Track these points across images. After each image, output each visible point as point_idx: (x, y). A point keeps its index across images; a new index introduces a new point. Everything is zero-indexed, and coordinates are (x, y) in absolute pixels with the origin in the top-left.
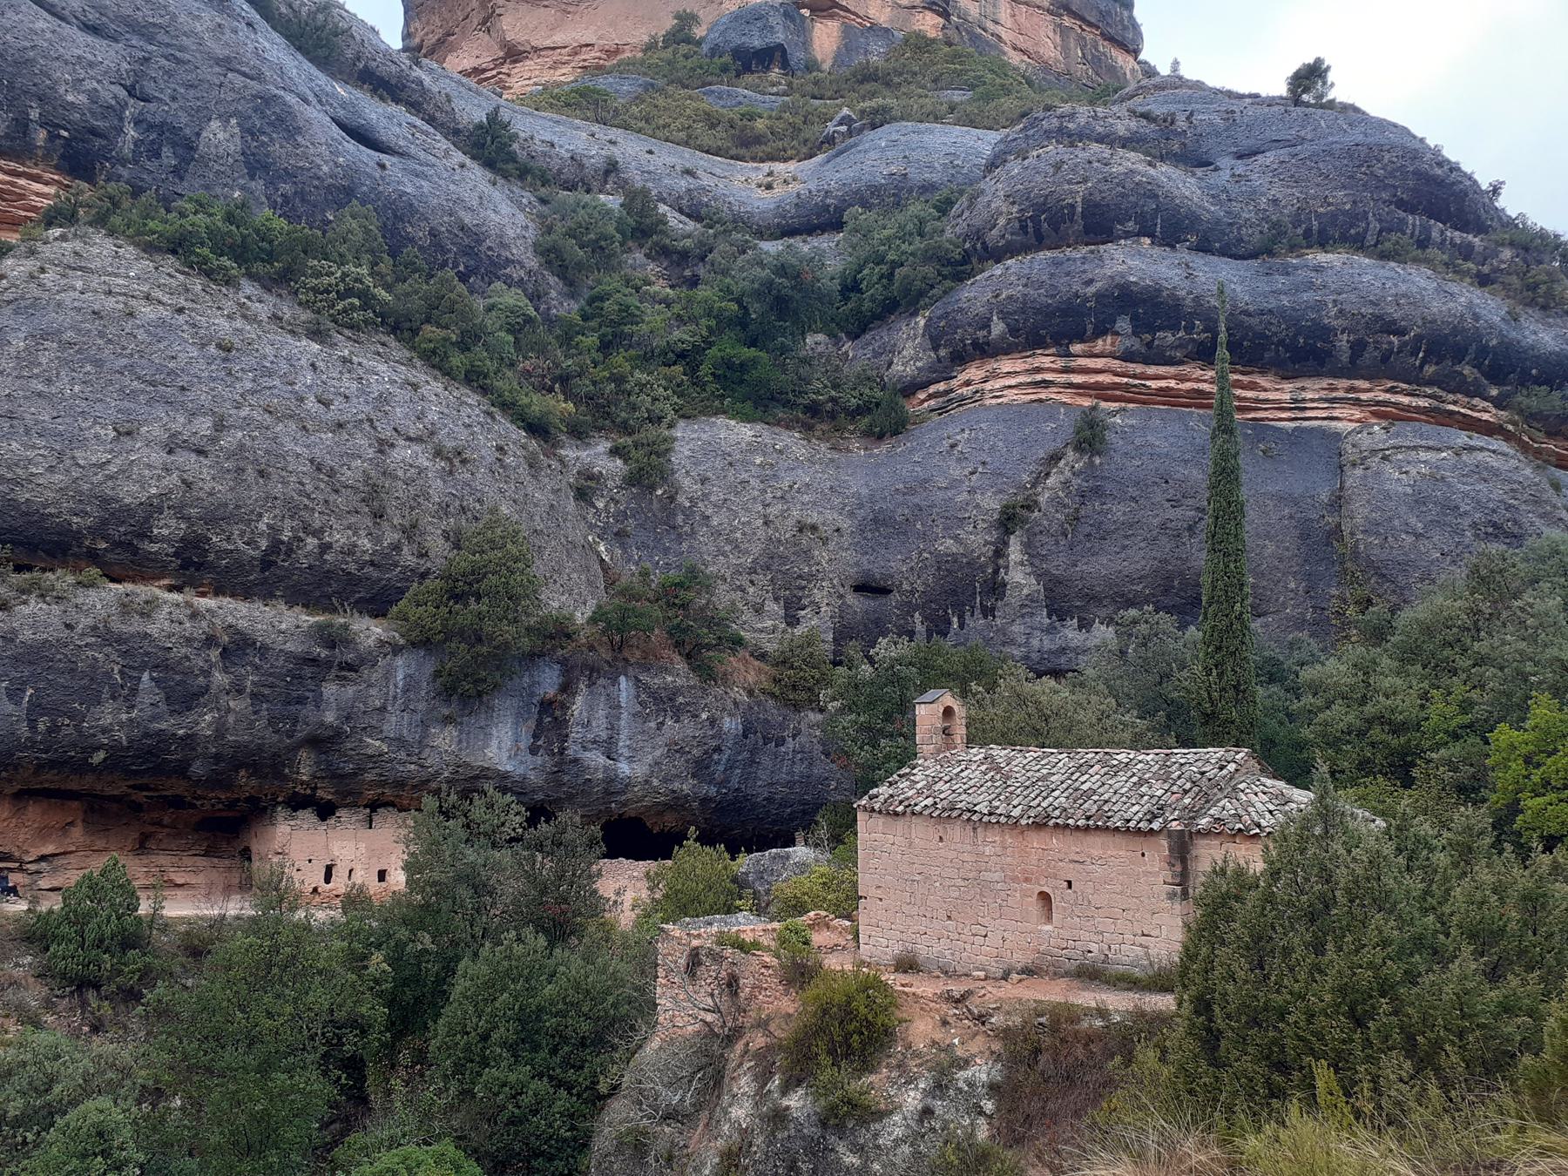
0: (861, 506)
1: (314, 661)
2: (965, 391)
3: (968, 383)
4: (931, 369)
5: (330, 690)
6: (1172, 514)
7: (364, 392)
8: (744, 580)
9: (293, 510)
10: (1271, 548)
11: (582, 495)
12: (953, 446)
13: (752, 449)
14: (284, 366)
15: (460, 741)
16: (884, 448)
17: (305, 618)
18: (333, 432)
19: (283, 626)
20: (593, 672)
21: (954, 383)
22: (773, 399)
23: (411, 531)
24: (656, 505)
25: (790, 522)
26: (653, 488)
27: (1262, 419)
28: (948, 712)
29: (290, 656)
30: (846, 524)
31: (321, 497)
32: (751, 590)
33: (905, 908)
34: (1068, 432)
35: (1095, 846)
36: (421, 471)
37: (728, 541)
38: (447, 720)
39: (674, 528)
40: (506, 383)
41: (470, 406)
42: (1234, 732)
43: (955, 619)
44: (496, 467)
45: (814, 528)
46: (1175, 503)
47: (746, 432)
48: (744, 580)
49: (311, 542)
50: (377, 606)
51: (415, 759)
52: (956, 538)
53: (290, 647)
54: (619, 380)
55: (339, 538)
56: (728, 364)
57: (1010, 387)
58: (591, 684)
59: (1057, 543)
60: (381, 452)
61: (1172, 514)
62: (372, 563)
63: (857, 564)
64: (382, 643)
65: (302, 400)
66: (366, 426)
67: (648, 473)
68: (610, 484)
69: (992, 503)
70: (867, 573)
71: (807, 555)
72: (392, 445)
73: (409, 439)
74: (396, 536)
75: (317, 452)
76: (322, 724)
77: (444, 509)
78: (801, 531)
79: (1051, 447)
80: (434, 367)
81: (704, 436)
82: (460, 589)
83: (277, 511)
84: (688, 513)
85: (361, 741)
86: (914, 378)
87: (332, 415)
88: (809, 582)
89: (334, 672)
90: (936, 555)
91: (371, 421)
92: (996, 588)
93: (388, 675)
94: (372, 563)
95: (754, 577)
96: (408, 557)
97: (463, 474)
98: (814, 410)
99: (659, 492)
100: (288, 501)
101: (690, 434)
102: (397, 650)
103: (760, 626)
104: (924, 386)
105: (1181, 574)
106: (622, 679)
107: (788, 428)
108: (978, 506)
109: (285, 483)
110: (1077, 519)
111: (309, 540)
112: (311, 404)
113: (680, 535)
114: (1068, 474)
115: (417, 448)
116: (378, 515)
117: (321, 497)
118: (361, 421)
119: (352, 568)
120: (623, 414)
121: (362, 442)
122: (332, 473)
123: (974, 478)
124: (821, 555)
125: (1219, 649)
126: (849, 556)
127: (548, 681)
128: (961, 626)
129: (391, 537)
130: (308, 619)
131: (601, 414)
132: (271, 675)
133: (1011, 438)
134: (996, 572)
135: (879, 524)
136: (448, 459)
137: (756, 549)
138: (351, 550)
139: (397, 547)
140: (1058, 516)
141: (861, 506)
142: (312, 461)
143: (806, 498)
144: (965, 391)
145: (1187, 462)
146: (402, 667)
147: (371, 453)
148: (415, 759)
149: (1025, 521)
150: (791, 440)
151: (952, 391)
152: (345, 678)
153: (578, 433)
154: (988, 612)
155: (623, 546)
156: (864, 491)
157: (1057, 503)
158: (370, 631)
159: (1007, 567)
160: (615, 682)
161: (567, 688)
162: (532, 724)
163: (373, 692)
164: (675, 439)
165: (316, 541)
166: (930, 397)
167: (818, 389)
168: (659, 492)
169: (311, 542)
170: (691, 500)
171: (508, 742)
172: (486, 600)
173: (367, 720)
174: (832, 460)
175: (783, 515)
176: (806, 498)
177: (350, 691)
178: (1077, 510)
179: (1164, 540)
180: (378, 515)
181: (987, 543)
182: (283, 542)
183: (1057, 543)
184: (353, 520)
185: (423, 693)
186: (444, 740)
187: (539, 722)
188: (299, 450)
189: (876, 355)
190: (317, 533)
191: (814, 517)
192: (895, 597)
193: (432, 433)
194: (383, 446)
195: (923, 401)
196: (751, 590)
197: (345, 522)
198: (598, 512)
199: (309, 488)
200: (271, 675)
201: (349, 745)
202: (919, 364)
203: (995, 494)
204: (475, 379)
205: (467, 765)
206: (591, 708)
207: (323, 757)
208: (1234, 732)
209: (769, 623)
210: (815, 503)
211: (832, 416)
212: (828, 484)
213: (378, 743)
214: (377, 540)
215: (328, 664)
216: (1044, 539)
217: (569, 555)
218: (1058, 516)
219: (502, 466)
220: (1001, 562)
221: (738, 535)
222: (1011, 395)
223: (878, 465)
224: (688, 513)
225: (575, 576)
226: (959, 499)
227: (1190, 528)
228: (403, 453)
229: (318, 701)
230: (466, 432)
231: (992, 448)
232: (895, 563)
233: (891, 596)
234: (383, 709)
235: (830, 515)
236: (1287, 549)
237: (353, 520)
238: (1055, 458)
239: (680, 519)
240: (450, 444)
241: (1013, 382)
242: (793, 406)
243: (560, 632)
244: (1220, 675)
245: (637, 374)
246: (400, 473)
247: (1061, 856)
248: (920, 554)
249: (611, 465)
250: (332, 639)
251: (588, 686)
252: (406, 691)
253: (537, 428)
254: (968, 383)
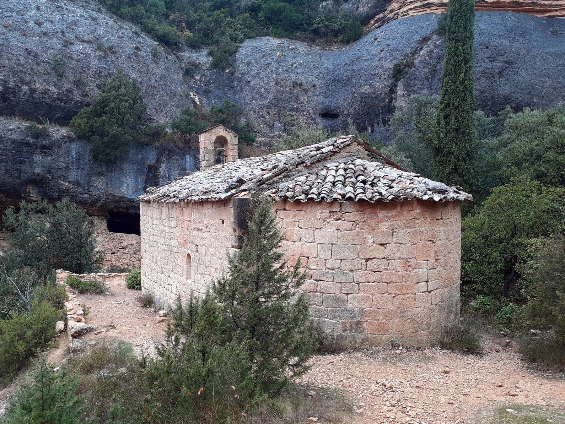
0: (328, 74)
1: (27, 144)
2: (391, 15)
3: (392, 11)
4: (375, 7)
5: (38, 158)
6: (488, 65)
7: (63, 20)
8: (264, 112)
9: (15, 73)
10: (549, 82)
11: (188, 73)
12: (375, 39)
13: (276, 48)
14: (21, 7)
15: (107, 184)
16: (348, 47)
17: (23, 124)
18: (40, 37)
19: (11, 127)
20: (170, 153)
21: (387, 12)
22: (298, 28)
23: (78, 84)
24: (225, 77)
25: (289, 82)
26: (224, 69)
27: (554, 16)
28: (221, 141)
29: (14, 141)
30: (319, 82)
31: (29, 66)
32: (268, 117)
34: (435, 26)
36: (87, 56)
37: (258, 93)
38: (101, 174)
39: (233, 88)
40: (151, 22)
41: (126, 29)
42: (453, 159)
43: (369, 128)
44: (133, 56)
45: (301, 85)
46: (491, 59)
47: (276, 42)
48: (264, 112)
49: (25, 88)
50: (64, 121)
51: (86, 191)
52: (370, 85)
53: (14, 137)
54: (218, 22)
55: (39, 86)
56: (274, 12)
57: (411, 9)
58: (169, 158)
59: (423, 84)
60: (65, 46)
61: (488, 65)
62: (59, 99)
63: (323, 103)
64: (64, 137)
65: (26, 22)
66: (60, 35)
67: (223, 62)
68: (204, 68)
69: (389, 64)
70: (328, 107)
71: (297, 98)
72: (72, 44)
73: (84, 41)
74: (70, 86)
75: (29, 46)
76: (34, 174)
77: (98, 74)
78: (294, 87)
79: (424, 33)
80: (114, 13)
81: (255, 45)
82: (101, 109)
83: (5, 73)
84: (240, 81)
85: (58, 182)
86: (368, 13)
87: (43, 28)
88: (297, 112)
89: (39, 150)
90: (360, 94)
91: (63, 32)
92: (390, 110)
93: (68, 152)
94: (59, 99)
95: (269, 110)
96: (77, 95)
97: (112, 58)
98: (317, 33)
99: (227, 71)
100: (11, 68)
101: (249, 44)
102: (71, 140)
103: (272, 134)
104: (373, 16)
105: (493, 98)
106: (188, 156)
107: (301, 41)
108: (382, 67)
109: (10, 59)
110: (435, 71)
111: (24, 87)
112: (31, 24)
113: (235, 91)
114: (432, 47)
115: (87, 46)
116: (61, 76)
117: (29, 66)
118: (57, 32)
119: (48, 101)
120: (217, 37)
121: (55, 42)
122: (36, 56)
123: (382, 53)
124: (304, 98)
125: (448, 105)
126: (319, 99)
127: (151, 157)
128: (373, 131)
129: (66, 86)
130: (24, 124)
131: (205, 38)
132: (4, 150)
133: (405, 32)
134: (390, 101)
135: (335, 82)
136: (105, 52)
137: (271, 96)
138: (47, 92)
139: (70, 91)
140: (425, 70)
141: (328, 74)
142: (26, 50)
143: (299, 70)
144: (391, 15)
145: (500, 36)
146: (74, 149)
147: (59, 46)
148: (86, 191)
149: (407, 73)
150: (301, 47)
151: (385, 17)
152: (46, 153)
153: (194, 46)
154: (385, 123)
155: (207, 97)
156: (331, 66)
157: (425, 63)
158: (57, 132)
159: (396, 98)
160: (183, 157)
161: (159, 161)
162: (144, 177)
163: (60, 159)
164: (241, 47)
165: (27, 88)
166: (376, 22)
167: (318, 22)
168: (227, 71)
169: (25, 88)
170: (242, 74)
171: (132, 185)
172: (108, 115)
173: (59, 173)
174: (319, 54)
175: (286, 79)
176: (299, 70)
177: (49, 159)
178: (435, 66)
179: (483, 79)
180: (61, 76)
181: (386, 86)
182: (10, 88)
183: (423, 84)
184: (46, 77)
185: (87, 161)
186: (99, 183)
187: (148, 176)
188: (19, 44)
189: (353, 5)
190: (28, 84)
191: (302, 80)
192: (341, 118)
193: (98, 39)
194: (67, 44)
195: (374, 24)
196: (268, 117)
197: (42, 79)
198: (196, 81)
199: (23, 62)
200: (4, 150)
201: (53, 184)
202: (370, 5)
203: (392, 60)
204: (136, 19)
205: (112, 195)
206: (170, 170)
207: (41, 189)
208: (453, 159)
209: (277, 133)
210: (304, 73)
211: (326, 35)
212: (312, 64)
213: (66, 184)
214: (59, 88)
215: (35, 146)
216: (416, 82)
217: (171, 98)
218: (425, 70)
219: (136, 56)
220: (393, 96)
221: (263, 90)
222: (411, 13)
223: (342, 54)
224: (240, 81)
225: (174, 108)
226: (374, 64)
227: (500, 73)
228: (79, 47)
229: (31, 163)
230: (118, 40)
231: (393, 38)
232: (341, 101)
233: (339, 118)
234: (67, 168)
235: (311, 78)
236: (559, 83)
237: (46, 77)
238: (426, 39)
239: (236, 83)
240: (107, 45)
241: (412, 6)
242: (305, 30)
243: (157, 134)
244: (447, 124)
245: (229, 19)
246: (74, 56)
248: (353, 94)
249: (207, 59)
250: (44, 134)
251: (168, 159)
252: (78, 159)
253: (164, 40)
254: (392, 11)
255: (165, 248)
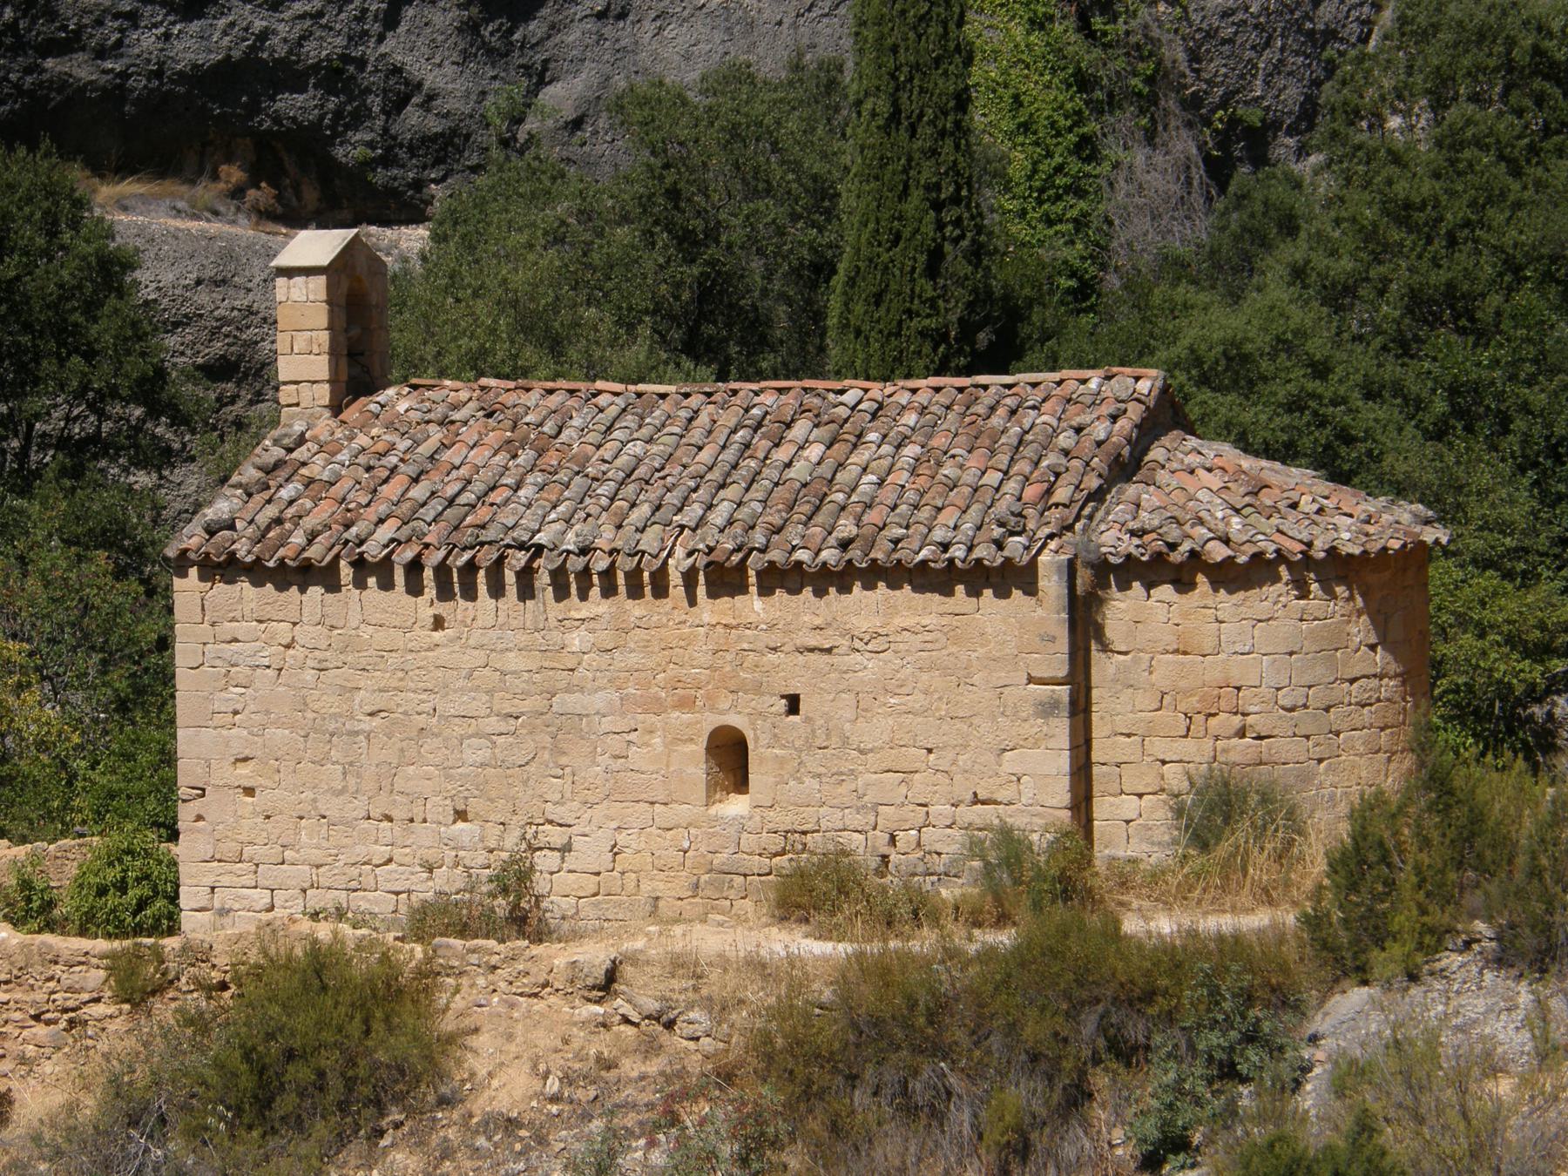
33: (331, 806)
35: (864, 607)
247: (775, 639)
255: (494, 724)
